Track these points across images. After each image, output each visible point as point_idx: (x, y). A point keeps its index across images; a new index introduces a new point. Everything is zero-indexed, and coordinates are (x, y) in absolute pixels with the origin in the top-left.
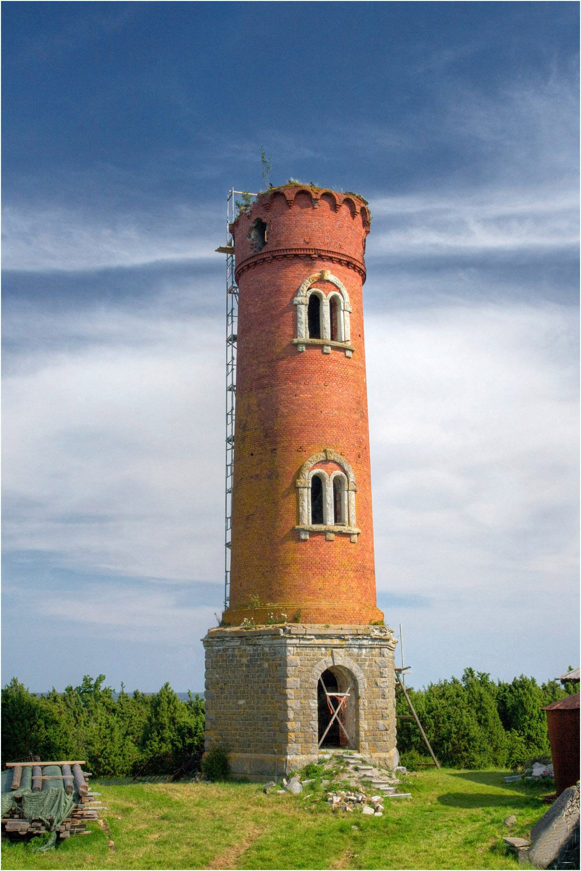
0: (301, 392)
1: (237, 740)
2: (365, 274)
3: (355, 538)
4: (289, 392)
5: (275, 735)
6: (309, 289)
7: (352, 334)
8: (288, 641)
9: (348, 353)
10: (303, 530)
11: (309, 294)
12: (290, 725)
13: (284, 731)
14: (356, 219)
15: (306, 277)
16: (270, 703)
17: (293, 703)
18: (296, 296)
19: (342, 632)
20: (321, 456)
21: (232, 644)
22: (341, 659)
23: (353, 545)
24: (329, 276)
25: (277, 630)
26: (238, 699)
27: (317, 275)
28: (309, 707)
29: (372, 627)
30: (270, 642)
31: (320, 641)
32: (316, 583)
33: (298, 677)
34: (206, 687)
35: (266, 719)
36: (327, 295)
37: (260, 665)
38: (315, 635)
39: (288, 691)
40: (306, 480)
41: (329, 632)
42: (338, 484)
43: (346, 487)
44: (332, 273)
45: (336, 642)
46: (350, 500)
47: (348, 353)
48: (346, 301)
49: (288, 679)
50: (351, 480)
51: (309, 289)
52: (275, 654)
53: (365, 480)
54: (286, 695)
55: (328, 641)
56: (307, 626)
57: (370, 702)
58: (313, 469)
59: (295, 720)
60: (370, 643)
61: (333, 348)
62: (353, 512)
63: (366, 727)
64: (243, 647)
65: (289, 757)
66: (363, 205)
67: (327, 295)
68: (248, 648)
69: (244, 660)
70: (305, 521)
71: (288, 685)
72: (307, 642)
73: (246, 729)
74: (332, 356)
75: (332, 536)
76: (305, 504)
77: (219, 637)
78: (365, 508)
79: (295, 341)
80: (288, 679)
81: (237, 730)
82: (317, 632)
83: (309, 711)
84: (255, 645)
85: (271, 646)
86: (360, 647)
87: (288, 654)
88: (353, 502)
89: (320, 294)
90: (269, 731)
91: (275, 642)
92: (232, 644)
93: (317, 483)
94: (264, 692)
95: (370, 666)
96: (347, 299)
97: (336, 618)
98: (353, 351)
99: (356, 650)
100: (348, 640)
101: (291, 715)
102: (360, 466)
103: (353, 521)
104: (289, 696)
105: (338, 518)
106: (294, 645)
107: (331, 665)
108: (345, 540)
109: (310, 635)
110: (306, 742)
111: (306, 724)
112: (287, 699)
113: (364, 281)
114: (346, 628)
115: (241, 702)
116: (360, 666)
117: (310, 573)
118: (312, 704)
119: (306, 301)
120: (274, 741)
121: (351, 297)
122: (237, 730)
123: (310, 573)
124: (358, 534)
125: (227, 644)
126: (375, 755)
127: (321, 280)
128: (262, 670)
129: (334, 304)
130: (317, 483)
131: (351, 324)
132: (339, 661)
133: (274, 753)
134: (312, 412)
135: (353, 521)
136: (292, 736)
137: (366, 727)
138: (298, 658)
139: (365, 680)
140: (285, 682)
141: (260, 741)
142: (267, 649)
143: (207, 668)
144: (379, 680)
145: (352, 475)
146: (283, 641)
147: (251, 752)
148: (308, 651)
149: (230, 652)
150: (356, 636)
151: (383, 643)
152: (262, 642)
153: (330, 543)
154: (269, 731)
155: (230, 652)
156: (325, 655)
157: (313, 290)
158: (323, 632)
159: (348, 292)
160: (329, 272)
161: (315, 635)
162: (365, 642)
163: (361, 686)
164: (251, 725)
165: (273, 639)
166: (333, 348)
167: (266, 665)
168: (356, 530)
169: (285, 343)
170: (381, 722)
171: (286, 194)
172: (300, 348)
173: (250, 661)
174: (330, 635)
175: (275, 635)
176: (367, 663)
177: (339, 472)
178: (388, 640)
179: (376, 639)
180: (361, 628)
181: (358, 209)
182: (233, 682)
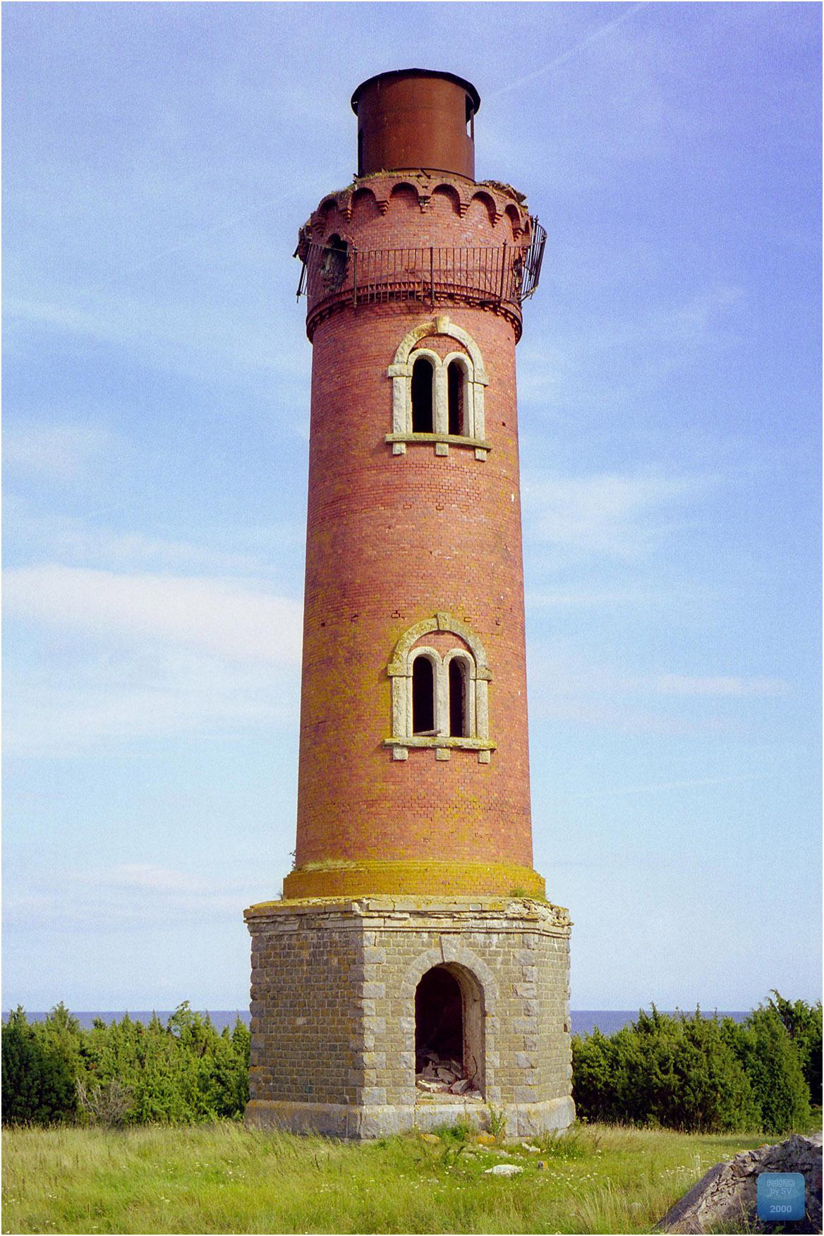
0: (399, 521)
1: (294, 1082)
2: (520, 326)
3: (486, 756)
4: (379, 522)
5: (346, 1073)
6: (413, 349)
7: (488, 422)
8: (366, 922)
9: (480, 454)
10: (397, 745)
11: (414, 357)
12: (367, 1058)
13: (359, 1067)
14: (498, 225)
15: (407, 330)
16: (340, 1022)
17: (373, 1023)
18: (392, 363)
19: (455, 908)
20: (430, 624)
21: (287, 928)
22: (456, 952)
23: (484, 768)
24: (447, 325)
25: (348, 904)
26: (297, 1015)
27: (426, 325)
28: (401, 1028)
29: (510, 900)
30: (340, 924)
31: (419, 922)
32: (418, 828)
33: (381, 980)
34: (252, 997)
35: (333, 1048)
36: (443, 358)
37: (326, 963)
38: (411, 913)
39: (365, 1003)
40: (404, 666)
41: (430, 908)
42: (458, 670)
43: (472, 675)
44: (453, 322)
45: (447, 923)
46: (478, 693)
47: (480, 454)
48: (476, 369)
49: (365, 985)
50: (480, 663)
51: (413, 349)
52: (347, 943)
53: (515, 661)
54: (361, 1009)
55: (432, 923)
56: (397, 898)
57: (504, 1022)
58: (416, 646)
59: (376, 1049)
60: (505, 924)
61: (452, 445)
62: (484, 715)
63: (497, 1063)
64: (304, 933)
65: (366, 1110)
66: (511, 201)
67: (443, 358)
68: (311, 934)
69: (305, 955)
70: (402, 732)
71: (365, 994)
72: (395, 923)
73: (307, 1065)
74: (451, 460)
75: (445, 754)
76: (403, 703)
77: (268, 917)
78: (513, 711)
79: (389, 437)
80: (365, 985)
81: (293, 1064)
82: (413, 908)
83: (399, 1036)
84: (319, 929)
85: (342, 931)
86: (489, 932)
87: (365, 943)
88: (484, 699)
89: (431, 358)
90: (338, 1067)
91: (347, 923)
92: (287, 928)
93: (423, 668)
94: (331, 1004)
95: (505, 962)
96: (480, 363)
97: (446, 886)
98: (488, 450)
99: (480, 938)
100: (466, 919)
101: (369, 1041)
102: (498, 639)
103: (484, 729)
104: (366, 1011)
105: (458, 727)
106: (378, 929)
107: (439, 961)
108: (469, 759)
109: (401, 912)
110: (396, 1084)
111: (394, 1058)
112: (362, 1015)
113: (518, 336)
114: (464, 901)
115: (300, 1021)
116: (489, 962)
117: (409, 814)
118: (405, 1025)
119: (409, 370)
120: (345, 1083)
121: (487, 361)
122: (293, 1064)
123: (409, 814)
124: (492, 750)
125: (281, 928)
126: (512, 1107)
127: (433, 333)
128: (330, 971)
129: (457, 373)
130: (423, 668)
131: (487, 406)
132: (451, 957)
133: (345, 1102)
134: (415, 553)
135: (484, 729)
136: (370, 1075)
137: (497, 1063)
138: (383, 950)
139: (497, 986)
140: (361, 988)
141: (325, 1082)
142: (336, 936)
143: (254, 968)
144: (521, 988)
145: (481, 655)
146: (357, 922)
147: (313, 1101)
148: (399, 938)
149: (285, 941)
150: (482, 914)
151: (527, 925)
152: (329, 925)
153: (443, 765)
154: (338, 1067)
155: (285, 941)
156: (429, 945)
157: (421, 351)
158: (423, 908)
159: (482, 351)
160: (446, 319)
161: (411, 913)
162: (495, 923)
163: (488, 995)
164: (312, 1057)
165: (344, 919)
166: (452, 445)
167: (335, 961)
168: (484, 741)
169: (374, 443)
170: (523, 1054)
171: (376, 191)
172: (400, 448)
173: (313, 955)
174: (435, 912)
175: (347, 913)
176: (500, 959)
177: (461, 652)
178: (535, 920)
179: (514, 919)
180: (488, 901)
181: (500, 208)
182: (290, 988)
